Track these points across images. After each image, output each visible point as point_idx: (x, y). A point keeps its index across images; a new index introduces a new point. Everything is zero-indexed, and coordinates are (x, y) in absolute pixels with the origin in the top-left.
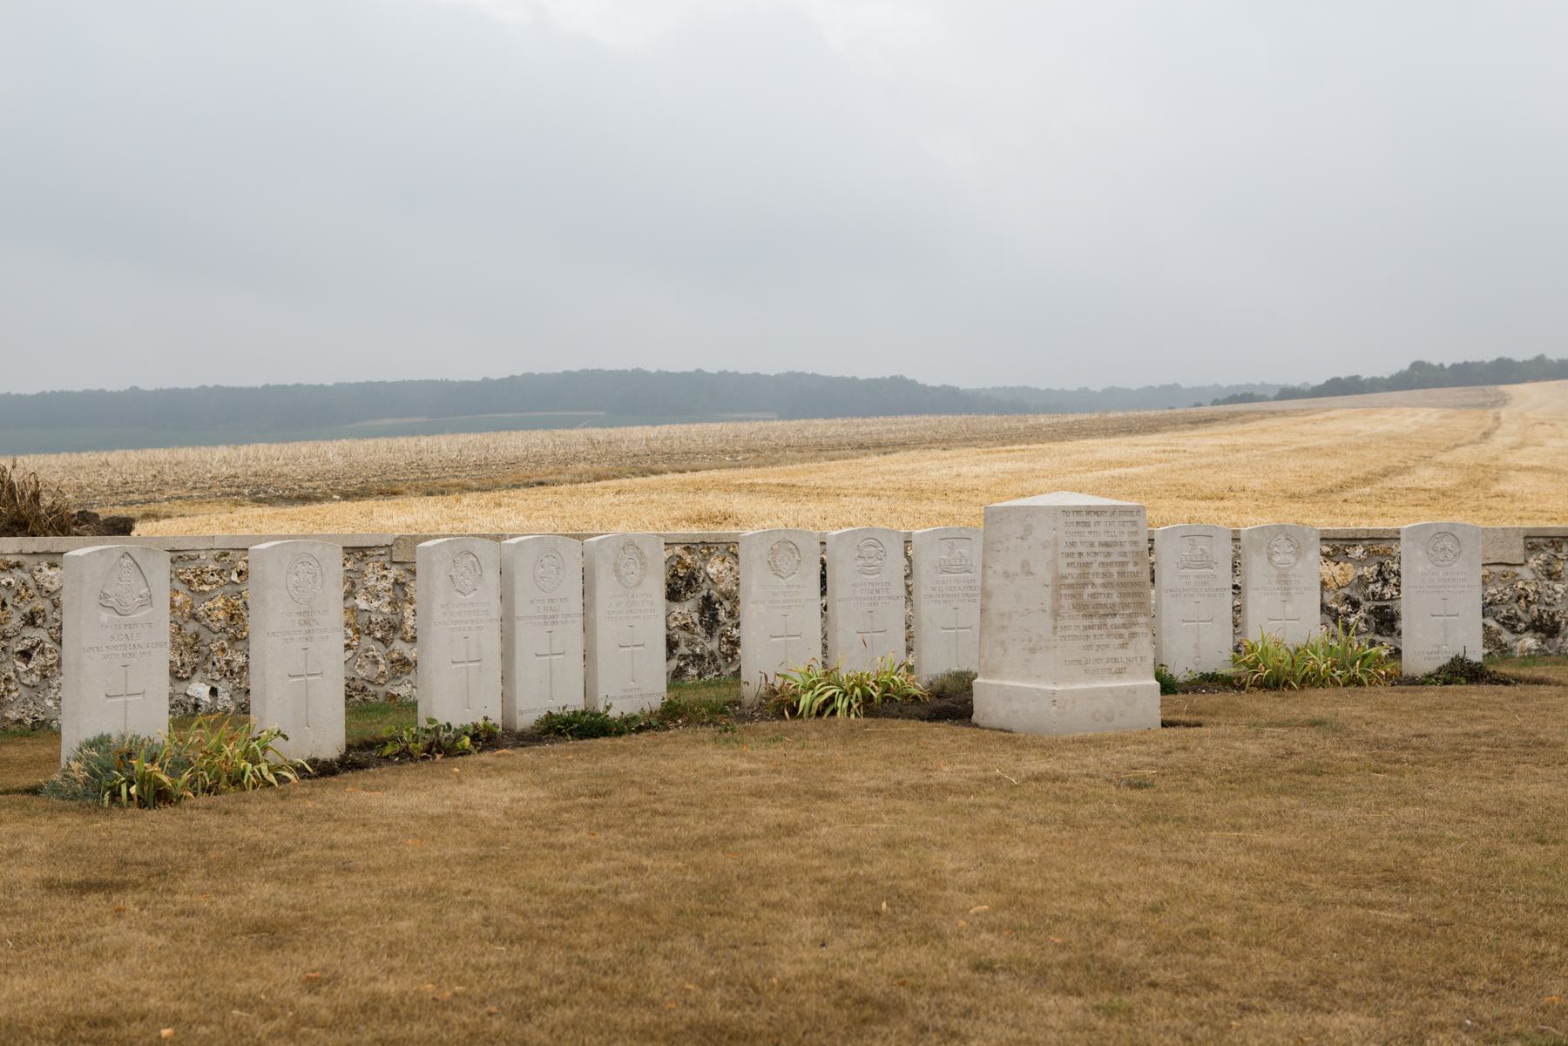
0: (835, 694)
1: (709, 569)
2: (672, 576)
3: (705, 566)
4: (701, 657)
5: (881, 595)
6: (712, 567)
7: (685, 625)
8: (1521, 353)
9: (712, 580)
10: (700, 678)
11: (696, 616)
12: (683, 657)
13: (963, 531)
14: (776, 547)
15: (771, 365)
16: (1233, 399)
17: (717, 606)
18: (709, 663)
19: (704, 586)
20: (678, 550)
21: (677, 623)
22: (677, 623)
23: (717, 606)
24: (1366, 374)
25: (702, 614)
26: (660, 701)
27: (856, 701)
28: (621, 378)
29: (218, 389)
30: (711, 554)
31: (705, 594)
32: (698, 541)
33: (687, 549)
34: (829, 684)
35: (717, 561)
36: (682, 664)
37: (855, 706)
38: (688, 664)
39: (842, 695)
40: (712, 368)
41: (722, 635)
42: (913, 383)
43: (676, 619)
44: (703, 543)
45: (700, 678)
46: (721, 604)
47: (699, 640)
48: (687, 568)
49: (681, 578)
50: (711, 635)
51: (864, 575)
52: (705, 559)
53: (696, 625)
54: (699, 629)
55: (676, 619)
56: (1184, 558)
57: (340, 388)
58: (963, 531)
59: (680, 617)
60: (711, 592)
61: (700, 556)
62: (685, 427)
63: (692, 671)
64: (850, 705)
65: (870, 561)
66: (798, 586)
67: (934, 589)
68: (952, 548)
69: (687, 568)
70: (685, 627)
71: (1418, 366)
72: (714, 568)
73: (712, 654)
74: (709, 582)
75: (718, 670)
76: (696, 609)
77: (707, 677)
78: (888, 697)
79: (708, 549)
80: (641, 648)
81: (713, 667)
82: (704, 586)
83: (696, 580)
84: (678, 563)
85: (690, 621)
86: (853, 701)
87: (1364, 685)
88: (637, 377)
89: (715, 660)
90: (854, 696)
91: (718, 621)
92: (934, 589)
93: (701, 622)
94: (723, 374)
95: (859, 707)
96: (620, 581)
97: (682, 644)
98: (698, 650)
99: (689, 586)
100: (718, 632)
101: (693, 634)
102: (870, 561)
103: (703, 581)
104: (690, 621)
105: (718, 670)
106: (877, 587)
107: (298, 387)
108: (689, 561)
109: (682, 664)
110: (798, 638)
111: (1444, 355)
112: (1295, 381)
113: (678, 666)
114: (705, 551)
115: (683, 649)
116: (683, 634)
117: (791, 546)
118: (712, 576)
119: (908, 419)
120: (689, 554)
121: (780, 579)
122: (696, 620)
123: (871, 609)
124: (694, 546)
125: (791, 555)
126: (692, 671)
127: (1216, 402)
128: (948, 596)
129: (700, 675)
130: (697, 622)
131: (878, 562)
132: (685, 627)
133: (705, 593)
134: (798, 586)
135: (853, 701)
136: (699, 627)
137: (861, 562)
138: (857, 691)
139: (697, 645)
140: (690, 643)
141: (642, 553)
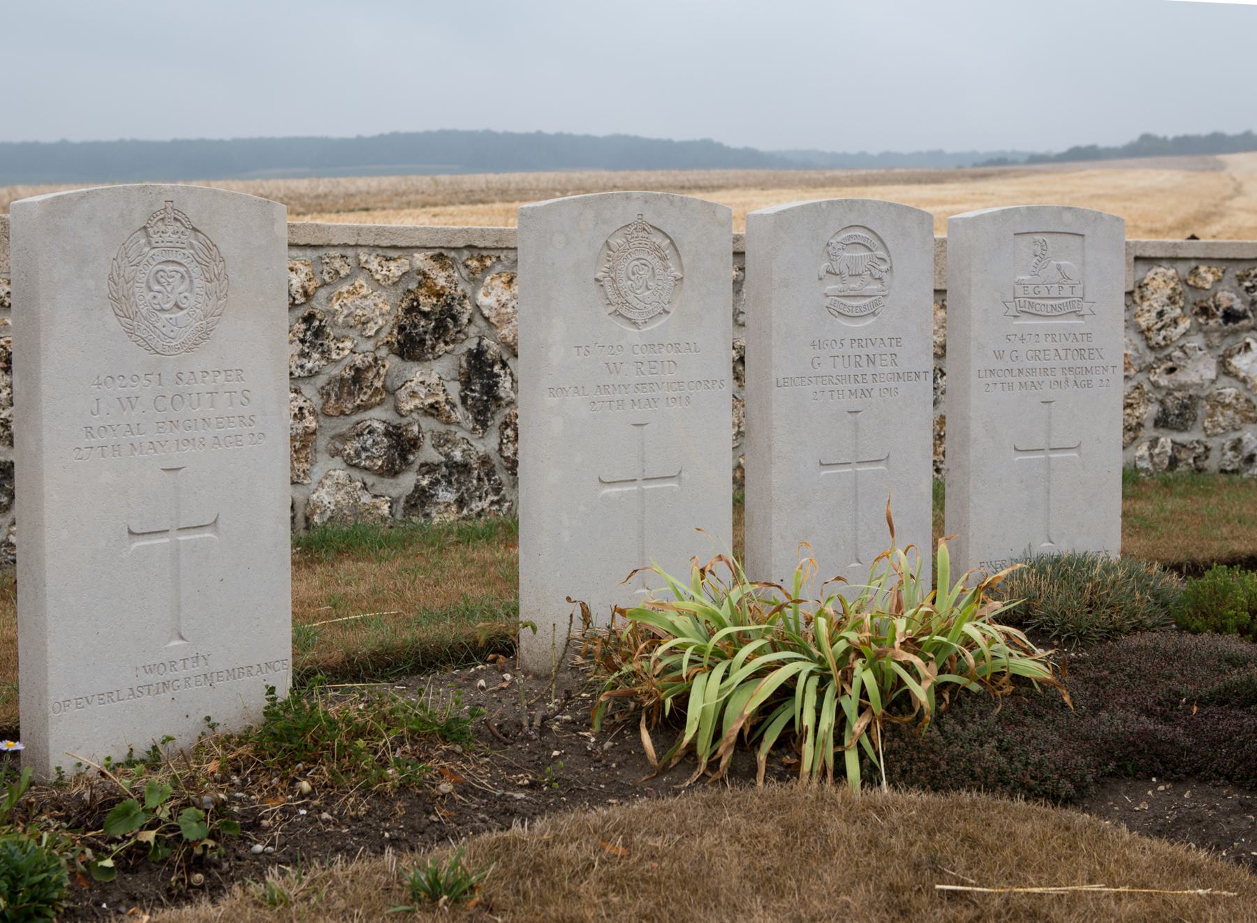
0: (794, 678)
1: (482, 299)
2: (408, 311)
3: (474, 292)
4: (465, 468)
5: (879, 369)
6: (487, 294)
7: (432, 406)
8: (1232, 129)
9: (487, 319)
10: (461, 508)
11: (454, 390)
12: (428, 468)
13: (1067, 217)
14: (617, 241)
15: (600, 128)
16: (991, 163)
17: (496, 369)
18: (479, 479)
19: (472, 331)
20: (420, 260)
21: (417, 402)
22: (417, 402)
23: (496, 369)
24: (1103, 143)
25: (467, 384)
26: (260, 702)
27: (861, 710)
28: (472, 136)
29: (135, 143)
30: (485, 270)
31: (474, 346)
32: (460, 244)
33: (439, 258)
34: (775, 648)
35: (497, 282)
36: (425, 482)
37: (858, 725)
38: (438, 482)
39: (814, 681)
40: (550, 130)
41: (506, 425)
42: (720, 145)
43: (414, 394)
44: (470, 247)
45: (461, 508)
46: (504, 365)
47: (460, 434)
48: (439, 295)
49: (426, 315)
50: (484, 425)
51: (842, 321)
52: (475, 279)
53: (453, 406)
54: (459, 414)
55: (414, 394)
56: (1020, 293)
57: (236, 143)
58: (1067, 217)
59: (422, 391)
60: (486, 342)
61: (464, 272)
62: (524, 174)
63: (446, 495)
64: (841, 721)
65: (855, 284)
66: (676, 346)
67: (999, 355)
68: (1041, 257)
69: (439, 295)
70: (433, 410)
71: (1146, 138)
72: (490, 297)
73: (485, 461)
74: (482, 323)
75: (497, 491)
76: (455, 374)
77: (476, 506)
78: (945, 685)
79: (481, 259)
80: (207, 535)
81: (486, 486)
82: (472, 331)
83: (454, 318)
84: (420, 285)
85: (441, 398)
86: (850, 706)
87: (1240, 440)
88: (488, 137)
89: (490, 473)
90: (854, 691)
91: (498, 399)
92: (999, 355)
93: (464, 400)
94: (559, 136)
95: (868, 729)
96: (130, 332)
97: (427, 443)
98: (458, 455)
99: (440, 330)
100: (499, 419)
101: (448, 423)
102: (855, 284)
103: (470, 321)
104: (441, 398)
105: (497, 491)
106: (871, 350)
107: (202, 142)
108: (441, 282)
109: (425, 482)
110: (673, 484)
111: (1168, 130)
112: (1041, 149)
113: (416, 487)
114: (474, 264)
115: (428, 453)
116: (429, 424)
117: (658, 239)
118: (486, 313)
119: (718, 171)
120: (443, 268)
121: (633, 330)
122: (455, 397)
123: (855, 403)
124: (453, 254)
125: (657, 263)
126: (446, 495)
127: (975, 165)
128: (1032, 371)
129: (461, 503)
130: (457, 401)
131: (874, 287)
132: (433, 410)
133: (472, 344)
134: (676, 346)
135: (850, 706)
136: (460, 408)
137: (832, 286)
138: (864, 675)
139: (455, 444)
140: (442, 441)
141: (211, 247)
